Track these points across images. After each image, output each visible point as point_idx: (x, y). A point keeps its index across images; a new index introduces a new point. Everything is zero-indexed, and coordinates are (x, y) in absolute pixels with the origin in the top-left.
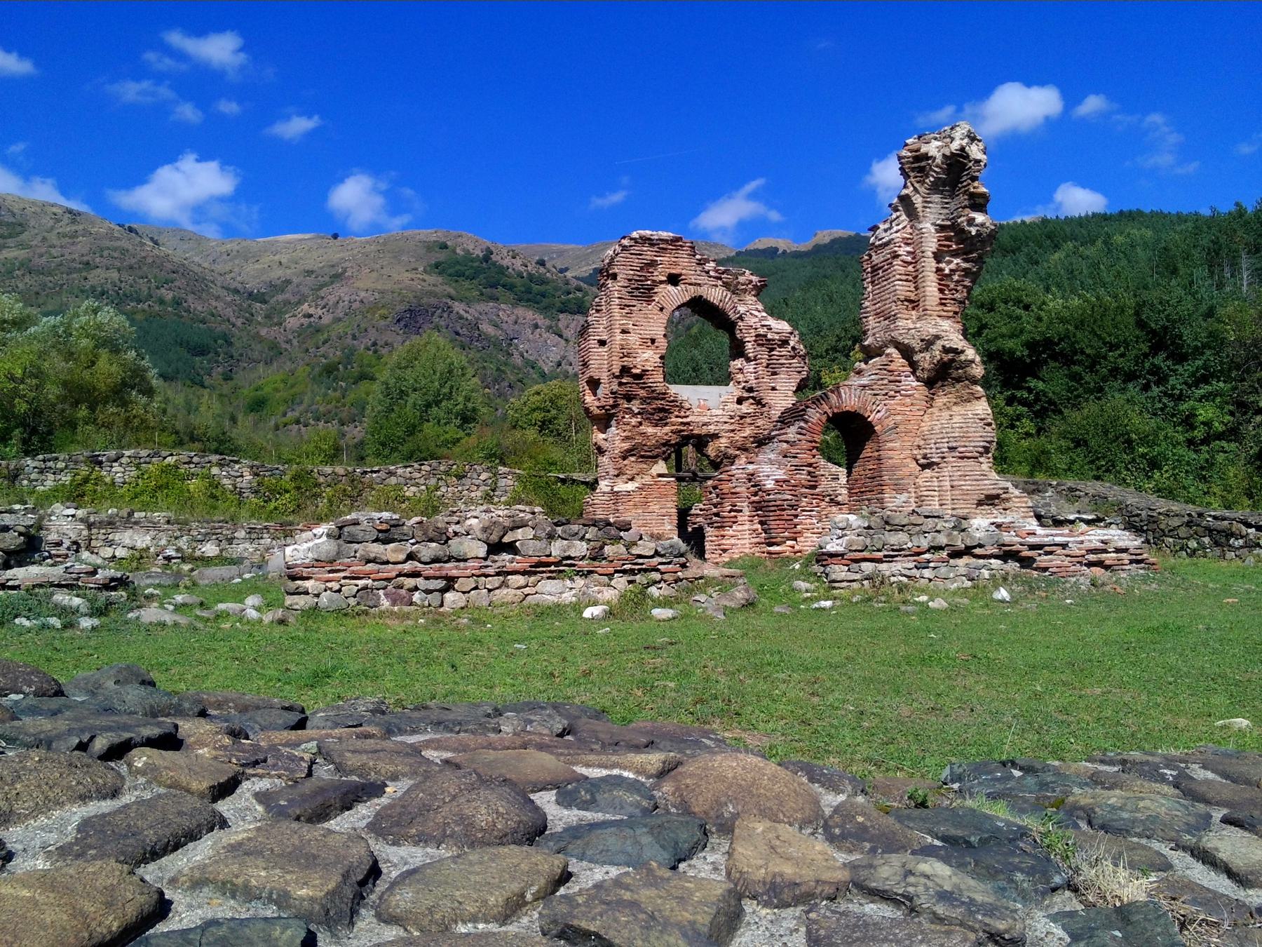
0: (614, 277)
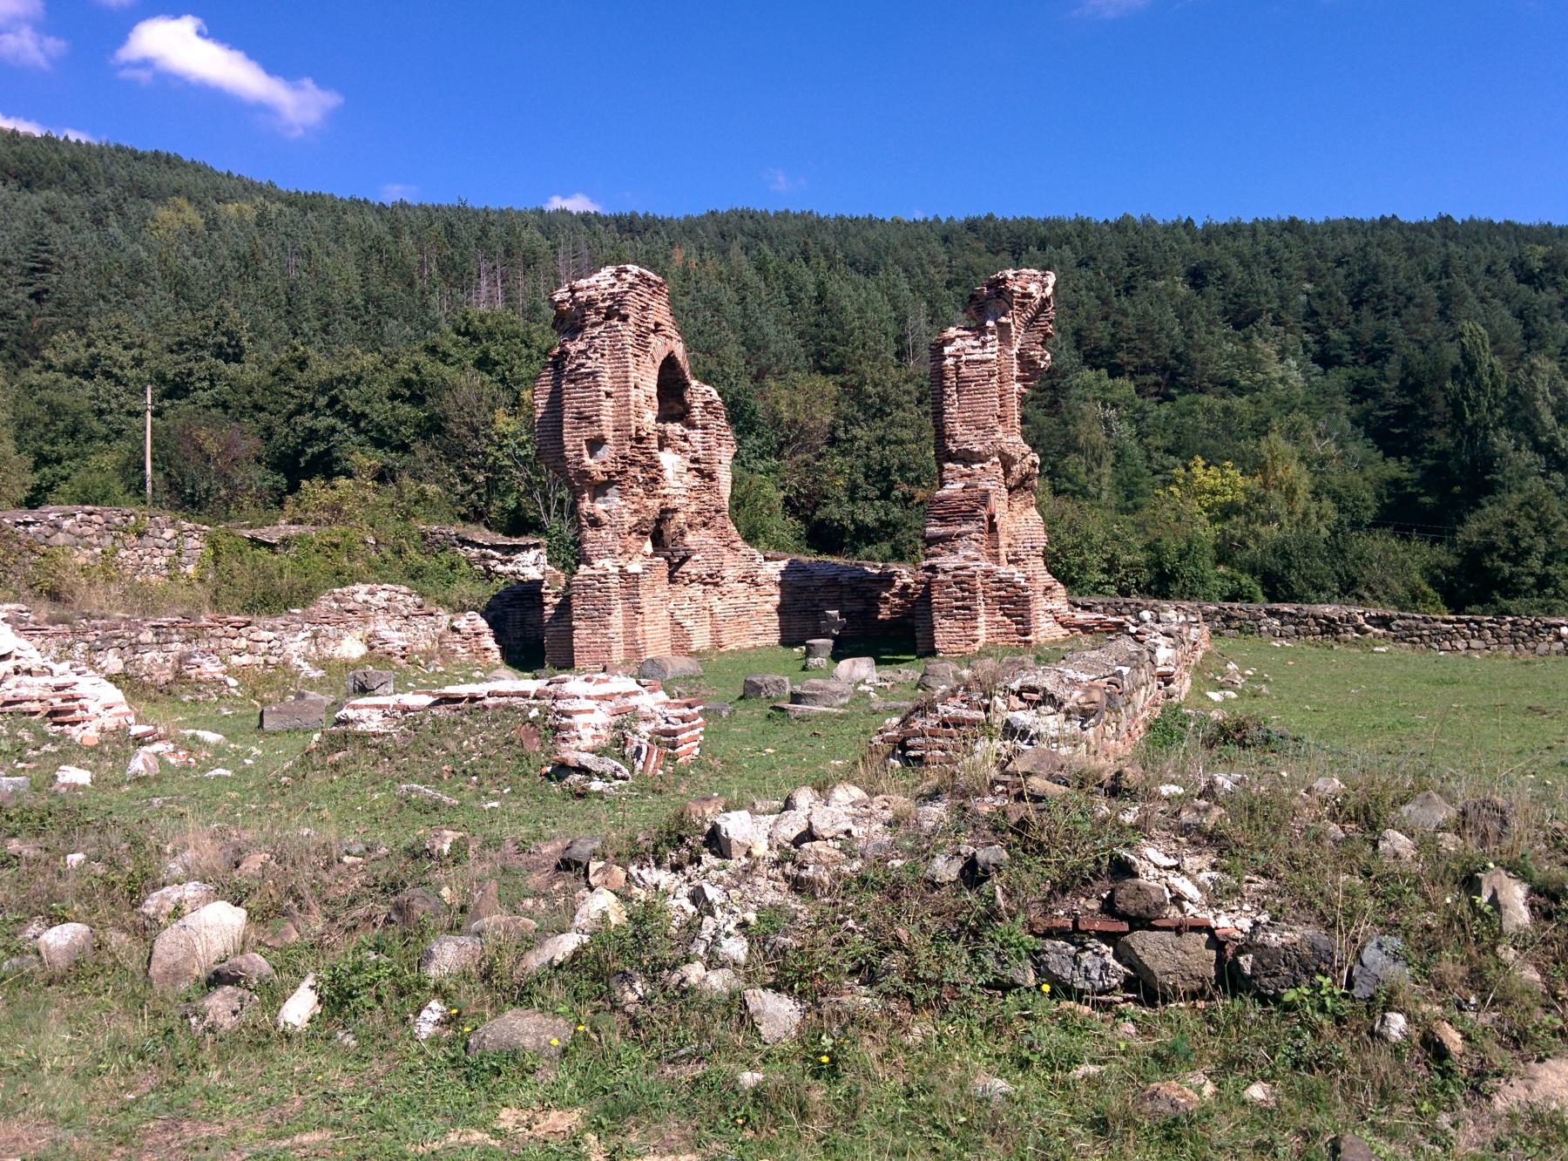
0: (624, 318)
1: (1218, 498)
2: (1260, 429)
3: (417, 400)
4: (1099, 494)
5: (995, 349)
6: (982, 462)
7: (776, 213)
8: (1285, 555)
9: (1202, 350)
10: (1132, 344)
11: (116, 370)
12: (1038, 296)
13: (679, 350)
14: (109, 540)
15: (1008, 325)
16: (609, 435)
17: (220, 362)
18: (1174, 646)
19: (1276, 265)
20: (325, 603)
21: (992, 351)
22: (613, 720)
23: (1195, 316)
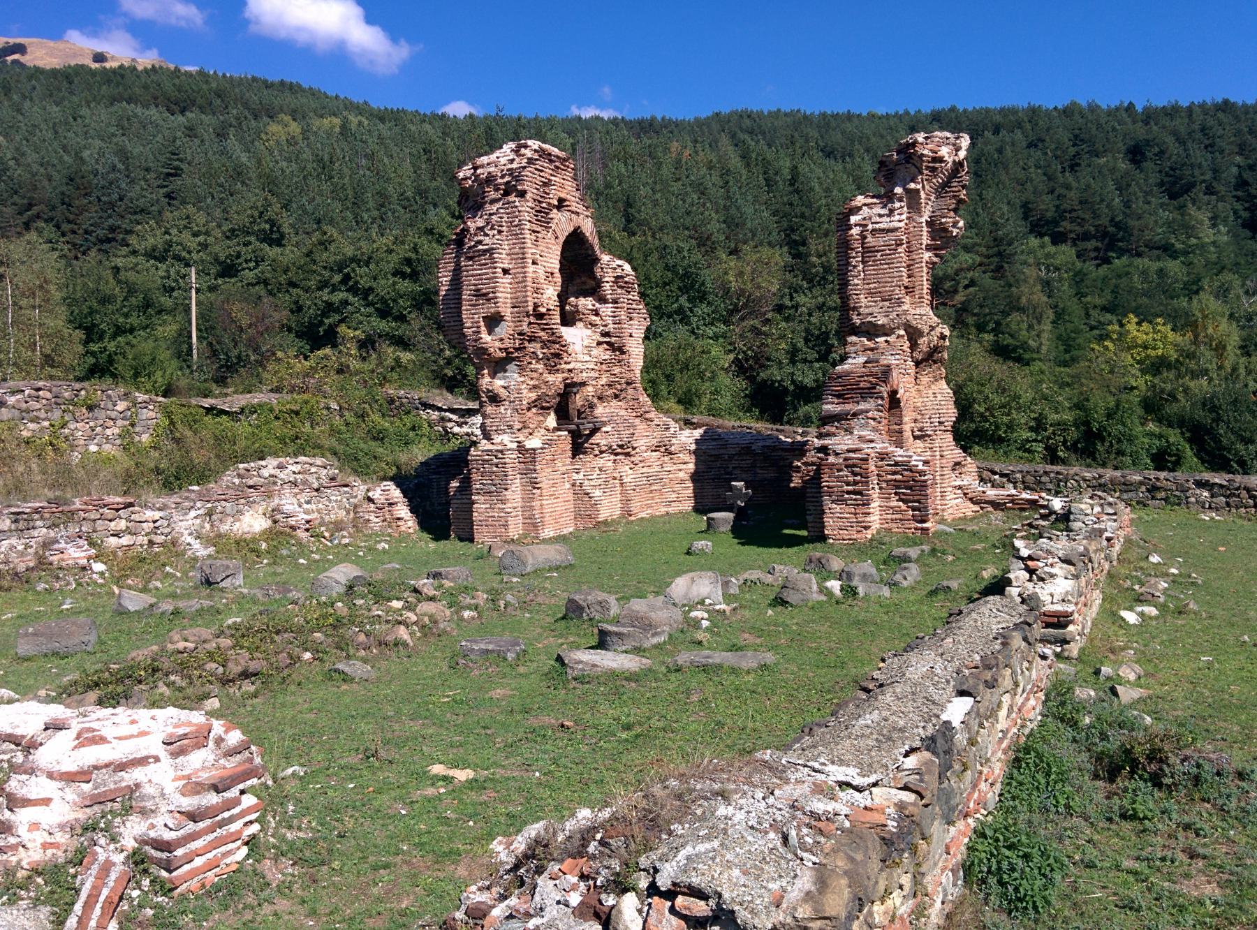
0: (522, 194)
1: (1149, 351)
2: (1192, 288)
3: (414, 276)
4: (1039, 348)
5: (904, 217)
6: (887, 335)
7: (770, 113)
8: (1214, 409)
9: (1139, 218)
10: (1074, 214)
11: (184, 254)
12: (950, 160)
13: (588, 227)
14: (57, 414)
15: (918, 191)
16: (507, 311)
17: (265, 246)
18: (1076, 577)
19: (1210, 141)
20: (230, 478)
21: (900, 219)
22: (82, 815)
23: (1134, 188)
